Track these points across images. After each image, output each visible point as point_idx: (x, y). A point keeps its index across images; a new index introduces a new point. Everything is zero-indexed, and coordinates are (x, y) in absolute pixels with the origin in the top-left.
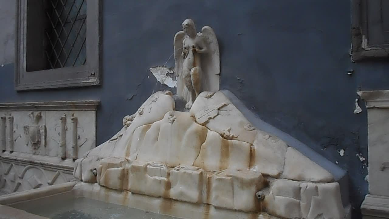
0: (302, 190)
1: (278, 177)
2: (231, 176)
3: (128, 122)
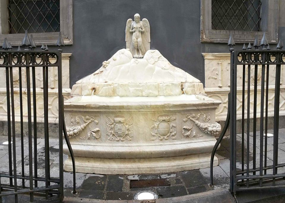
1: (186, 82)
2: (171, 83)
3: (107, 64)
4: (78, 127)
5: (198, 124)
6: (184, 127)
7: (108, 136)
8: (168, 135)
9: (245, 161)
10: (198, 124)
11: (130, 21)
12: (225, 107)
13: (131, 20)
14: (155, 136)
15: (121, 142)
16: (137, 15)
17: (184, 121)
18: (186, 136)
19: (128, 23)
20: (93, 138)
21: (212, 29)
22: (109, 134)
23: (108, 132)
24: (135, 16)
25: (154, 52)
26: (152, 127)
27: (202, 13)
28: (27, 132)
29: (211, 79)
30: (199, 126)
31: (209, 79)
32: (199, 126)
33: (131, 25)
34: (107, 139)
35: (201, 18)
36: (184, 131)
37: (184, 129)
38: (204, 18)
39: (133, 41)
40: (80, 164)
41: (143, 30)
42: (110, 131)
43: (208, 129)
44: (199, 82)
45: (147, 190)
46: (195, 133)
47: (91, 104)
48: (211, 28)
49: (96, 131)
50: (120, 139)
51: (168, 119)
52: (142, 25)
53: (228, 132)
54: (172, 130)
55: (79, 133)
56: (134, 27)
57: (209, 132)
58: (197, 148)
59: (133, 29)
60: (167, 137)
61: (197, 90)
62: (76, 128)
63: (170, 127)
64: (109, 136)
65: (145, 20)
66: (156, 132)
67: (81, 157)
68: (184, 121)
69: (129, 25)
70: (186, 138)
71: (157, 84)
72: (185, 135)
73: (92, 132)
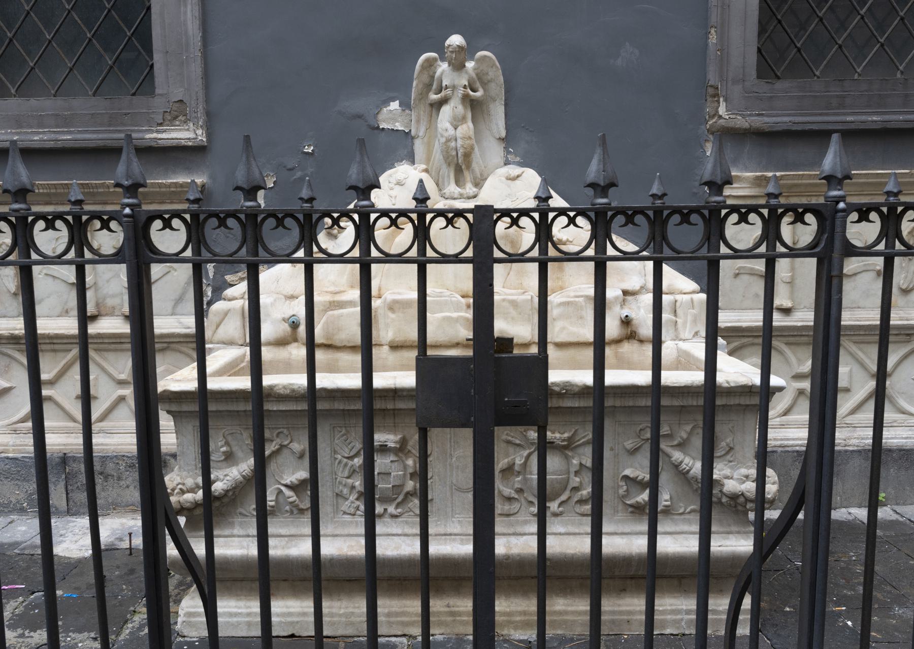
0: (678, 304)
4: (227, 471)
5: (681, 462)
6: (628, 472)
7: (340, 501)
8: (563, 497)
9: (878, 631)
10: (681, 462)
11: (430, 63)
12: (801, 392)
13: (435, 60)
14: (513, 498)
15: (389, 520)
16: (456, 40)
17: (628, 451)
18: (631, 506)
19: (423, 67)
20: (287, 508)
21: (759, 77)
22: (346, 491)
23: (340, 483)
24: (448, 42)
25: (518, 176)
26: (505, 467)
27: (714, 18)
28: (31, 494)
29: (745, 278)
30: (688, 471)
31: (737, 275)
32: (688, 471)
33: (433, 77)
34: (336, 510)
35: (713, 38)
36: (625, 488)
37: (626, 478)
38: (721, 37)
39: (442, 136)
40: (239, 608)
41: (479, 94)
42: (350, 481)
43: (723, 485)
44: (694, 292)
45: (818, 226)
46: (667, 497)
47: (276, 386)
48: (754, 73)
49: (296, 482)
50: (385, 510)
51: (564, 440)
52: (474, 76)
53: (728, 251)
54: (578, 479)
55: (231, 493)
56: (444, 85)
57: (724, 500)
58: (674, 554)
59: (440, 91)
60: (559, 507)
61: (685, 323)
62: (222, 477)
63: (573, 470)
64: (347, 499)
65: (485, 56)
66: (517, 486)
67: (242, 580)
68: (628, 451)
69: (425, 78)
70: (632, 512)
71: (529, 297)
72: (628, 502)
73: (283, 488)
